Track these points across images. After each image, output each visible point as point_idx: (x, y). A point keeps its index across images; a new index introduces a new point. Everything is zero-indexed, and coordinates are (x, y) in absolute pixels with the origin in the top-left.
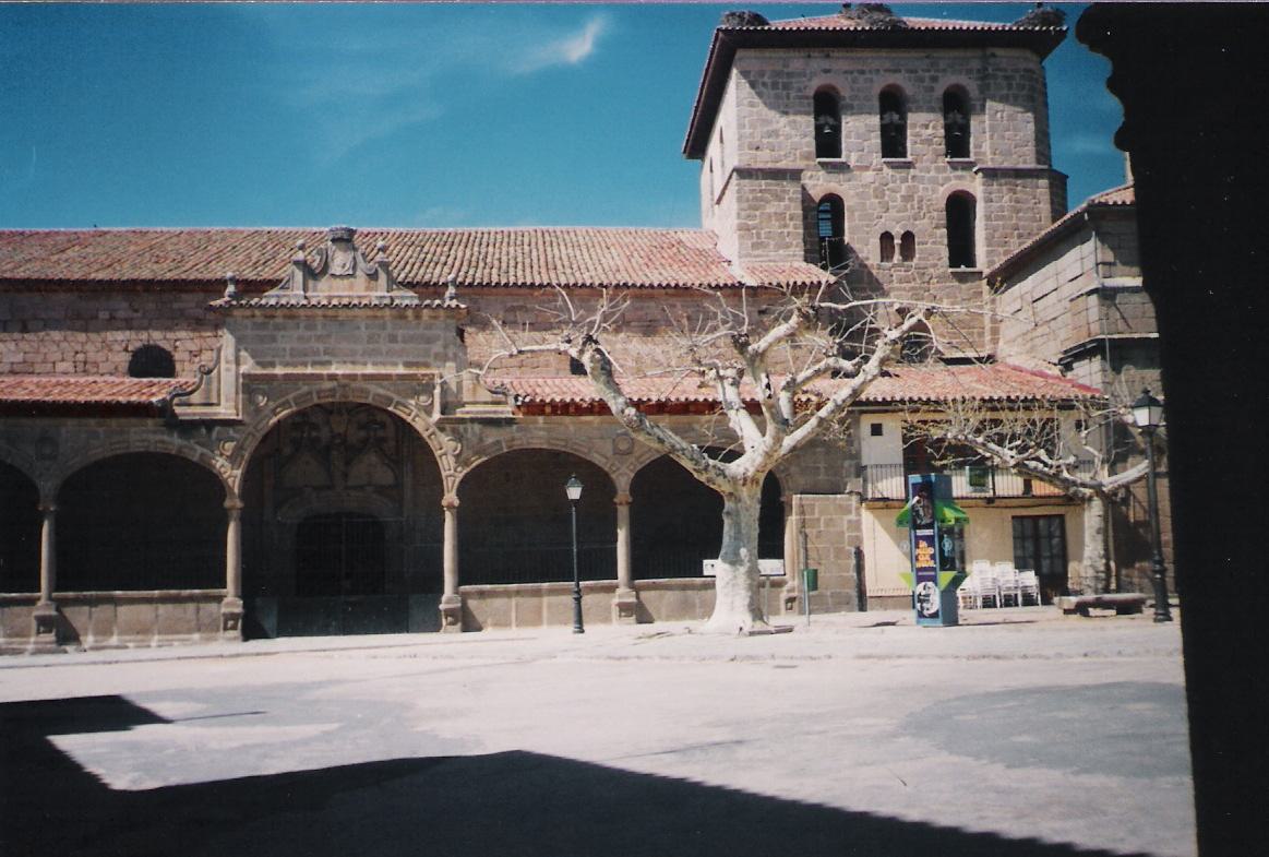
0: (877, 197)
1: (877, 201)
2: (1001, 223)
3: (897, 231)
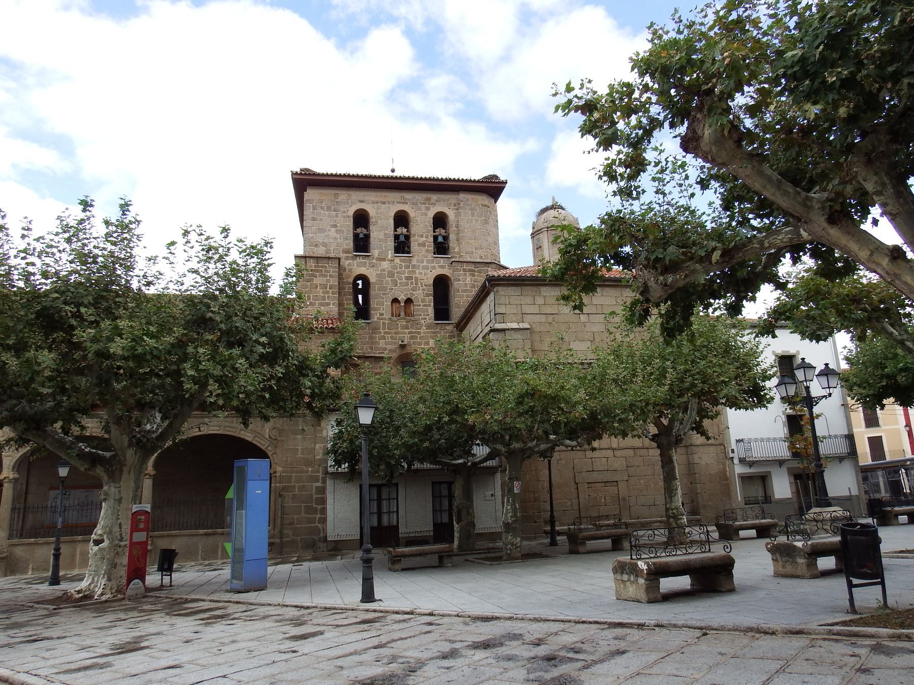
3: (402, 298)
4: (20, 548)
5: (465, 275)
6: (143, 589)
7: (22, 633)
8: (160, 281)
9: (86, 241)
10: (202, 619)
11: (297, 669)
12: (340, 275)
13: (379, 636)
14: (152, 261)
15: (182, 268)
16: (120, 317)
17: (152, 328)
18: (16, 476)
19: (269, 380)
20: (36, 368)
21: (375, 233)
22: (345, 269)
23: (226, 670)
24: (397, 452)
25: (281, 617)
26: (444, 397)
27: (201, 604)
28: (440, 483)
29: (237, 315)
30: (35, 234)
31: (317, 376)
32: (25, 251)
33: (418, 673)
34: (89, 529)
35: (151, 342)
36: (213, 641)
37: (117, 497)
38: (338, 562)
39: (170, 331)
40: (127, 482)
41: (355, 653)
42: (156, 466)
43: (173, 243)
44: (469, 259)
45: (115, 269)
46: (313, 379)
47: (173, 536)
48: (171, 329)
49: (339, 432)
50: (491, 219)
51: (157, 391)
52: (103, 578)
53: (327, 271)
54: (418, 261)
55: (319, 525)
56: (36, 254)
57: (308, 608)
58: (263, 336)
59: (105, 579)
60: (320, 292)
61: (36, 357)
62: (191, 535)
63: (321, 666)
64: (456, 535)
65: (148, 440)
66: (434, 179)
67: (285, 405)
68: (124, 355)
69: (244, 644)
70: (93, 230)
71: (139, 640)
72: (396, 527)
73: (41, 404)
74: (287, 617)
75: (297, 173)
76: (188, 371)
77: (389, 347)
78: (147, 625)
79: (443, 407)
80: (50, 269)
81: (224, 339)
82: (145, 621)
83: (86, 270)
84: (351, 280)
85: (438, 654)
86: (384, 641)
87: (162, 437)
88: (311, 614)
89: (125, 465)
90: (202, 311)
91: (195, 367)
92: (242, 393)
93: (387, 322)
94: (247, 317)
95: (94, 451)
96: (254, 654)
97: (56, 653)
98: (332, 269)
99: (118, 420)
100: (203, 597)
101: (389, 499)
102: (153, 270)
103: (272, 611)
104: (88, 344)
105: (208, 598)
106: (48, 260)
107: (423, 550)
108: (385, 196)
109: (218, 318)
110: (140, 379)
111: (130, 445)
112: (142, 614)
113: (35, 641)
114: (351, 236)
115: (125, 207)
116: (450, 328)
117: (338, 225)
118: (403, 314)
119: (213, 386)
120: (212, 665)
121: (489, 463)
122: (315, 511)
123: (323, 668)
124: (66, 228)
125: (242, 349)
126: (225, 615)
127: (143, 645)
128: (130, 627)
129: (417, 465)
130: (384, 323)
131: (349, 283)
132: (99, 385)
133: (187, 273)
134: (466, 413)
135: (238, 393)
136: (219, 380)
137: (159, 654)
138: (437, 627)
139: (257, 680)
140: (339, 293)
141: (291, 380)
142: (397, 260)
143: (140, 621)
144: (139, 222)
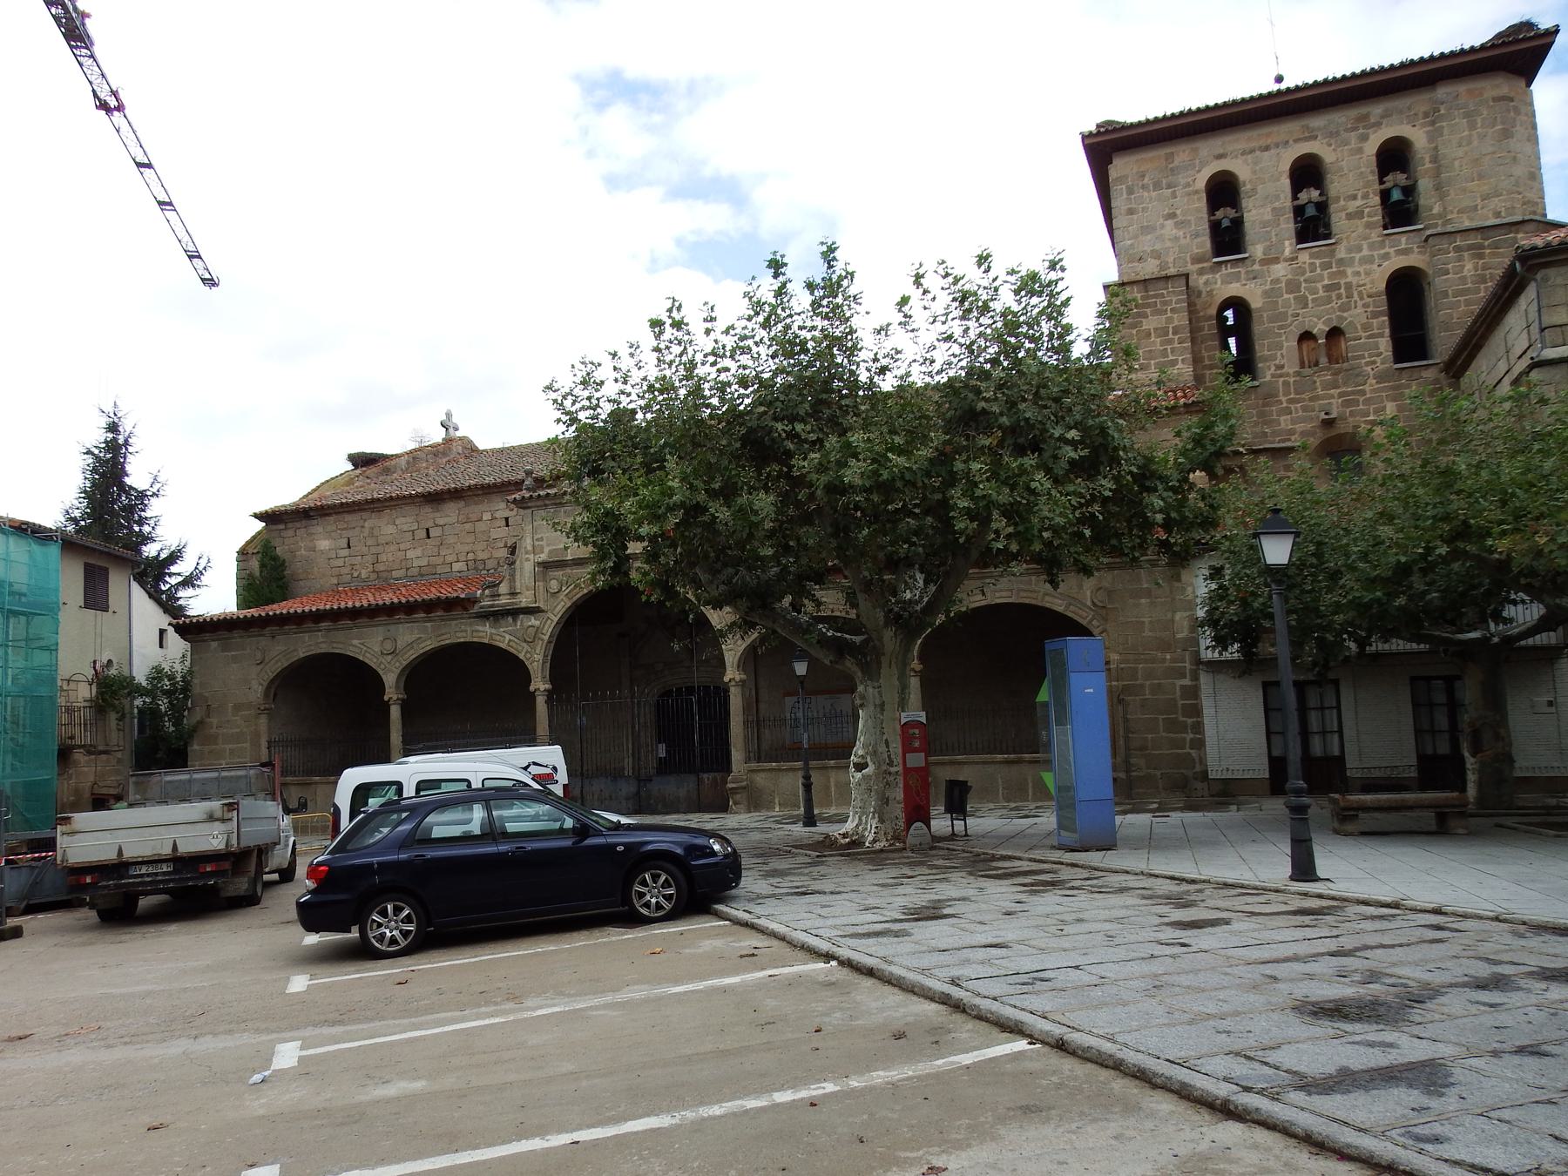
1: (1291, 296)
3: (1320, 328)
4: (763, 775)
5: (1460, 259)
6: (929, 838)
7: (786, 883)
8: (898, 363)
9: (788, 321)
10: (1024, 885)
11: (1196, 972)
12: (1191, 305)
13: (1337, 936)
14: (883, 333)
15: (929, 335)
16: (851, 429)
17: (897, 439)
18: (744, 677)
19: (1088, 503)
20: (753, 518)
21: (1254, 212)
22: (1200, 293)
23: (1079, 961)
24: (1339, 618)
25: (1150, 892)
26: (1435, 506)
27: (1017, 863)
28: (1428, 679)
29: (1024, 400)
30: (720, 326)
31: (1172, 489)
32: (713, 353)
33: (1429, 1005)
34: (844, 751)
35: (901, 461)
36: (1047, 916)
37: (878, 702)
38: (1232, 814)
39: (925, 439)
40: (889, 677)
41: (1295, 958)
42: (922, 658)
43: (904, 301)
44: (1467, 224)
45: (833, 356)
46: (1165, 494)
47: (960, 763)
48: (925, 436)
49: (1220, 588)
50: (1523, 119)
51: (915, 539)
52: (873, 818)
53: (1165, 303)
54: (1349, 250)
55: (1191, 751)
56: (728, 354)
57: (1193, 882)
58: (1071, 429)
59: (877, 819)
60: (1156, 342)
61: (750, 503)
62: (984, 763)
63: (1235, 971)
64: (1471, 777)
65: (911, 615)
66: (1373, 72)
67: (1121, 543)
68: (864, 485)
69: (1099, 926)
70: (793, 303)
71: (937, 905)
72: (1341, 760)
73: (763, 571)
74: (1160, 893)
75: (1091, 134)
76: (959, 502)
77: (1300, 427)
78: (944, 886)
79: (1433, 528)
80: (747, 372)
81: (1009, 441)
82: (940, 880)
83: (794, 366)
84: (1213, 311)
85: (1466, 979)
86: (1348, 947)
87: (931, 609)
88: (1201, 891)
89: (884, 654)
90: (969, 401)
91: (969, 493)
92: (1046, 530)
93: (1292, 380)
94: (1042, 399)
95: (839, 634)
96: (1117, 941)
97: (836, 911)
98: (1174, 297)
99: (867, 586)
100: (1017, 854)
101: (1322, 708)
102: (888, 345)
103: (1131, 881)
104: (814, 476)
105: (1026, 856)
106: (745, 359)
107: (1403, 800)
108: (1268, 135)
109: (996, 409)
110: (888, 521)
111: (886, 625)
112: (934, 871)
113: (804, 894)
114: (1205, 227)
115: (829, 254)
116: (1430, 374)
117: (1178, 212)
118: (1323, 360)
119: (999, 522)
120: (1054, 950)
121: (1540, 639)
122: (1183, 728)
123: (1242, 975)
124: (758, 306)
125: (1040, 455)
126: (1057, 882)
127: (946, 911)
128: (921, 886)
129: (1377, 646)
130: (1286, 384)
131: (1209, 318)
132: (835, 535)
133: (936, 343)
134: (1489, 534)
135: (1040, 531)
136: (1010, 512)
137: (972, 927)
138: (1455, 934)
139: (1131, 979)
140: (1193, 340)
141: (1128, 501)
142: (1304, 257)
143: (933, 881)
144: (852, 275)
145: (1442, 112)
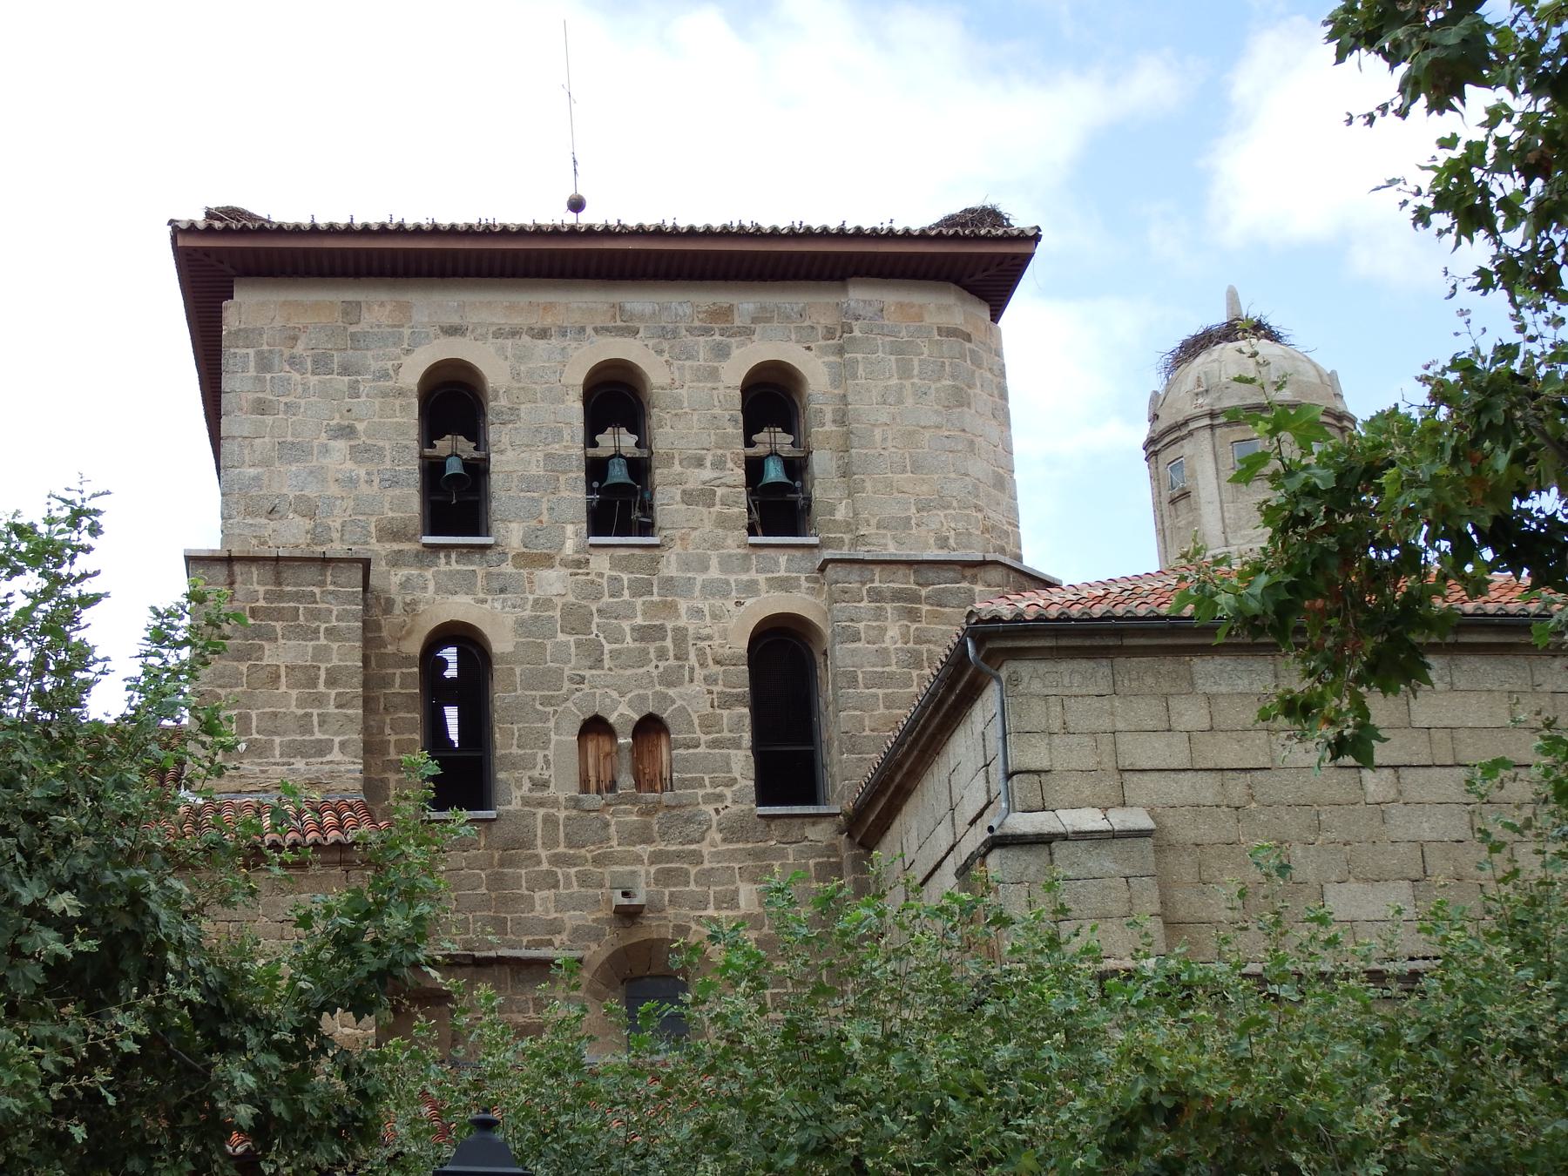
0: (572, 631)
2: (880, 692)
145: (857, 333)
